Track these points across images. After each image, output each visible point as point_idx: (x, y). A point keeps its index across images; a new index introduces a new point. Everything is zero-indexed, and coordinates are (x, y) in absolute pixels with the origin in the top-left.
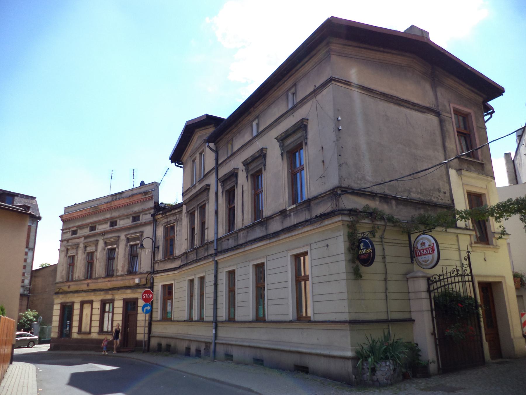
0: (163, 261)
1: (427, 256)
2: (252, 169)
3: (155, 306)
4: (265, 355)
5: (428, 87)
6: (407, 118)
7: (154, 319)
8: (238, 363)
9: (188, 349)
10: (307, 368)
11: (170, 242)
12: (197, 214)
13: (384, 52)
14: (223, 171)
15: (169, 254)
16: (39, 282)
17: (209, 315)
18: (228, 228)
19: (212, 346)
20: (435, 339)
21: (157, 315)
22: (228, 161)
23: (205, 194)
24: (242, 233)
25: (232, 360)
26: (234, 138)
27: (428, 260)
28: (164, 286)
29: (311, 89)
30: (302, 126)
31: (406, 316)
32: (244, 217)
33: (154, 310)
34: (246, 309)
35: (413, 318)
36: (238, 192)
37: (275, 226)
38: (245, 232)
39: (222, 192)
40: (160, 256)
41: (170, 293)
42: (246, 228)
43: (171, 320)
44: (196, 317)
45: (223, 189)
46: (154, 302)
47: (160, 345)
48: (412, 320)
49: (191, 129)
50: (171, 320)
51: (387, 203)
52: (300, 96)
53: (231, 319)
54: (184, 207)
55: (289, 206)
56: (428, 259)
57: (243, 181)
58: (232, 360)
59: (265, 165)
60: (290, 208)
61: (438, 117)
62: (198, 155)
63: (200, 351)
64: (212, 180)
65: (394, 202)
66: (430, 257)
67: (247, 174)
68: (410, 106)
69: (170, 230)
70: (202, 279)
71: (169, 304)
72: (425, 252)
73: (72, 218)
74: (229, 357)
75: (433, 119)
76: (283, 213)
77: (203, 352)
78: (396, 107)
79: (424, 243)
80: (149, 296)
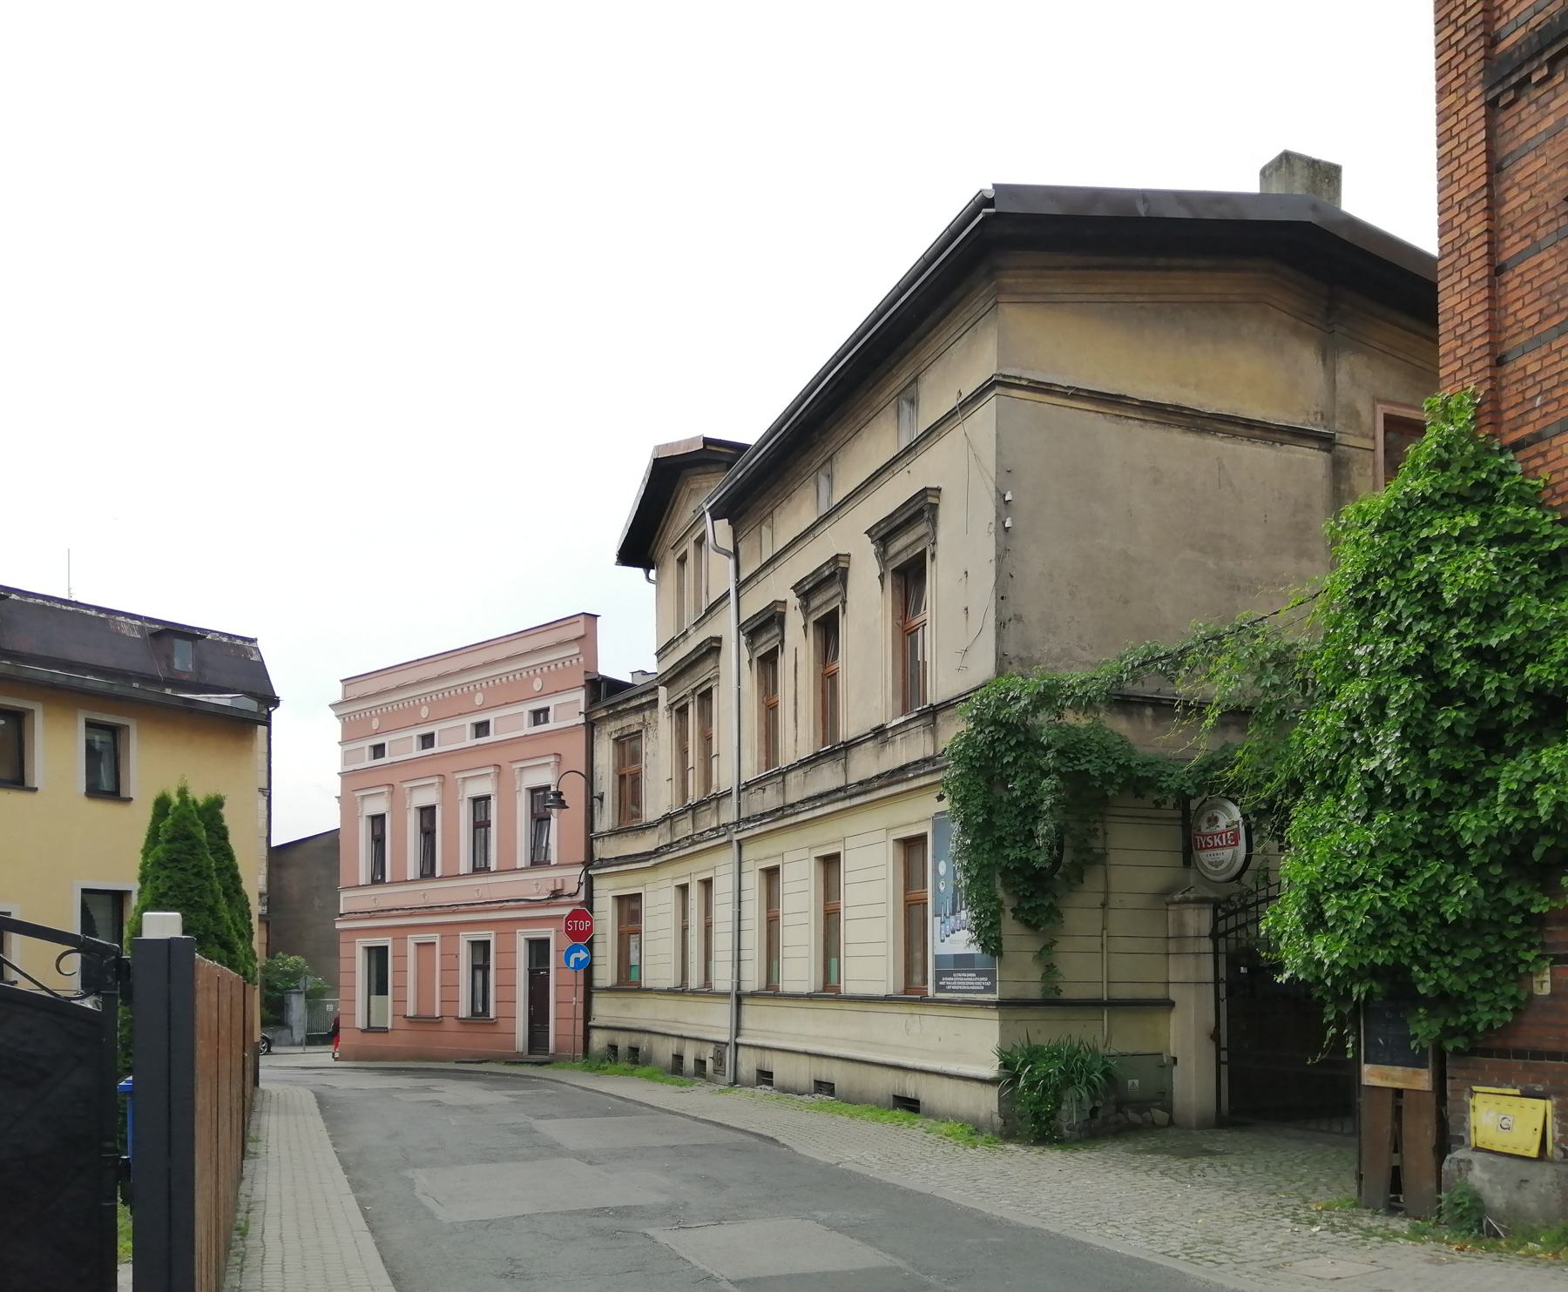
0: (614, 833)
1: (1219, 851)
2: (818, 608)
3: (598, 949)
4: (836, 1073)
5: (1307, 357)
6: (1221, 467)
7: (597, 983)
8: (785, 1090)
9: (679, 1058)
10: (917, 1102)
11: (630, 785)
12: (692, 711)
13: (1169, 269)
14: (755, 602)
15: (630, 820)
16: (293, 878)
17: (723, 979)
18: (764, 759)
19: (728, 1054)
20: (1218, 1050)
21: (605, 974)
22: (762, 576)
23: (709, 664)
24: (793, 774)
25: (770, 1083)
26: (776, 512)
27: (1222, 862)
28: (620, 899)
29: (951, 402)
30: (921, 510)
31: (1157, 993)
32: (797, 740)
33: (597, 961)
34: (799, 972)
35: (1172, 997)
36: (785, 663)
37: (865, 765)
38: (800, 772)
39: (750, 662)
40: (606, 820)
41: (636, 917)
42: (803, 763)
43: (640, 990)
44: (694, 981)
45: (752, 651)
46: (597, 939)
47: (613, 1048)
48: (1168, 1004)
49: (668, 476)
50: (640, 990)
51: (1129, 715)
52: (930, 413)
53: (771, 991)
54: (662, 691)
55: (894, 718)
56: (1221, 858)
57: (798, 639)
58: (770, 1083)
59: (844, 602)
60: (895, 723)
61: (1329, 451)
62: (690, 546)
63: (704, 1062)
64: (725, 626)
65: (1149, 711)
66: (1228, 852)
67: (806, 619)
68: (1238, 429)
69: (628, 747)
70: (707, 884)
71: (633, 944)
72: (1217, 840)
73: (368, 705)
74: (765, 1077)
75: (1314, 460)
76: (879, 732)
77: (710, 1065)
78: (1191, 439)
79: (1216, 819)
80: (583, 925)
